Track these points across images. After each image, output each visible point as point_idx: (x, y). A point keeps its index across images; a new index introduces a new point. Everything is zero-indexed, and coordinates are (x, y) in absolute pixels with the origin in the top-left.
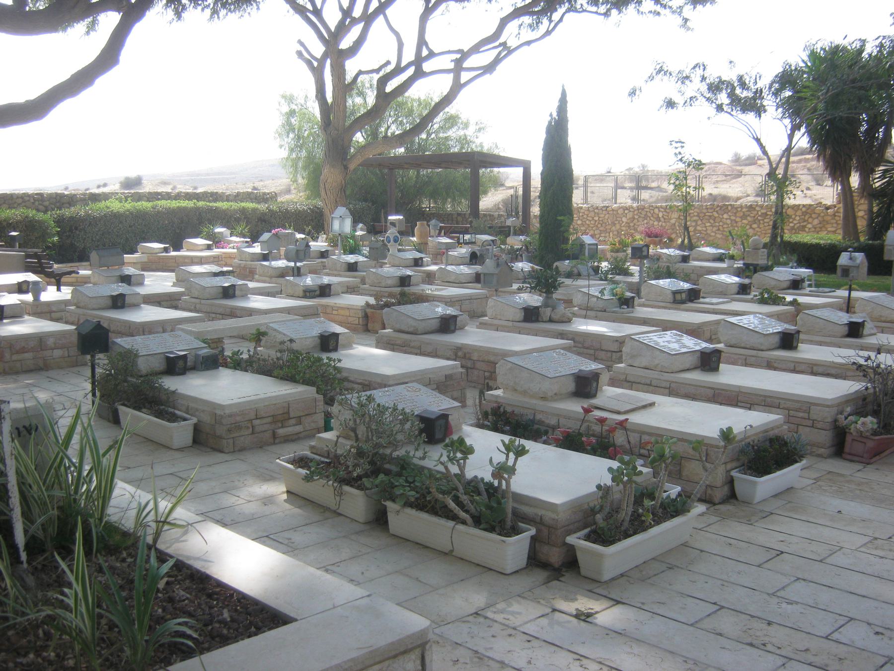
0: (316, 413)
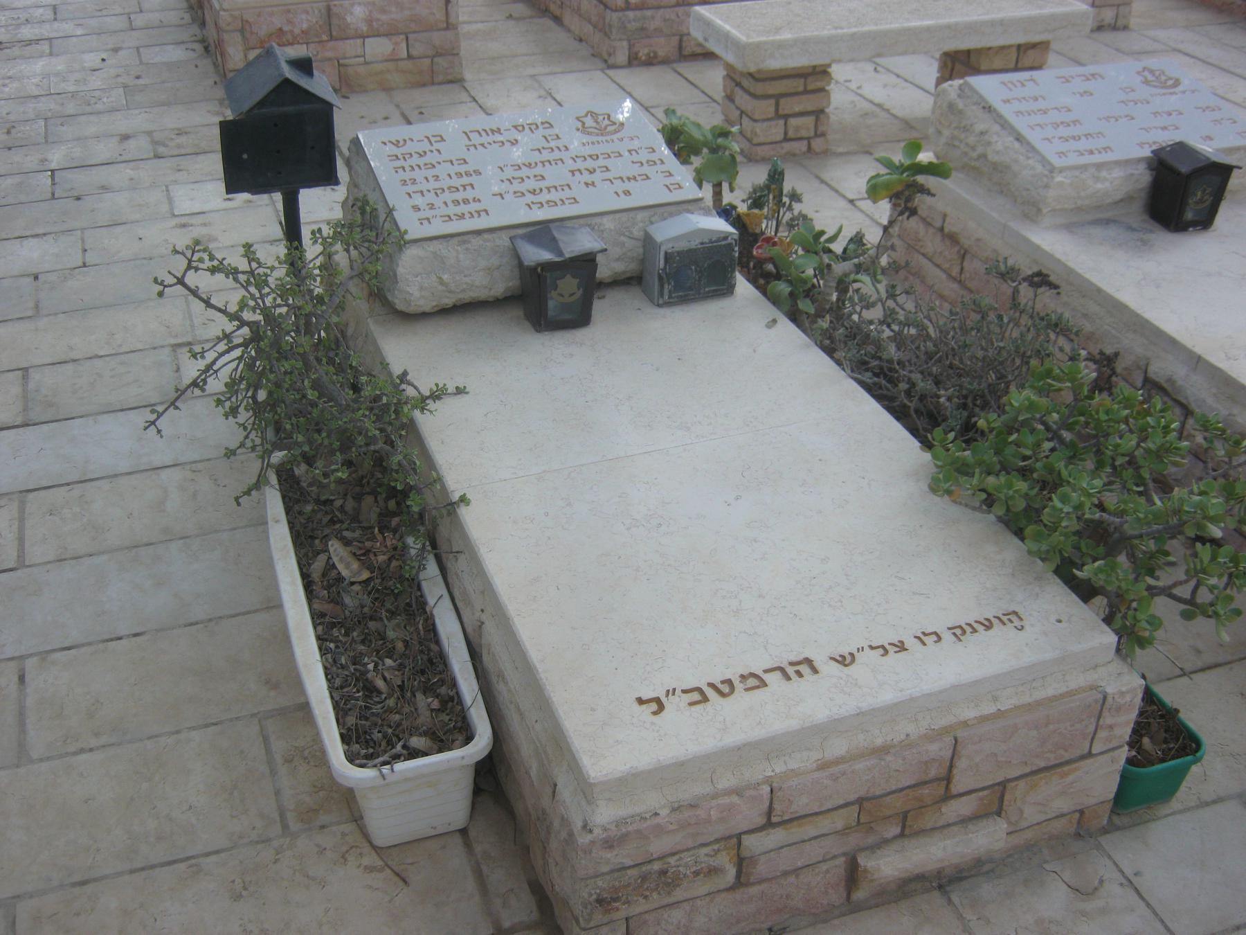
0: (1089, 755)
